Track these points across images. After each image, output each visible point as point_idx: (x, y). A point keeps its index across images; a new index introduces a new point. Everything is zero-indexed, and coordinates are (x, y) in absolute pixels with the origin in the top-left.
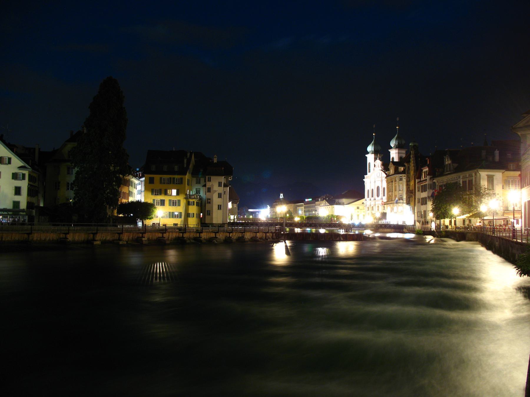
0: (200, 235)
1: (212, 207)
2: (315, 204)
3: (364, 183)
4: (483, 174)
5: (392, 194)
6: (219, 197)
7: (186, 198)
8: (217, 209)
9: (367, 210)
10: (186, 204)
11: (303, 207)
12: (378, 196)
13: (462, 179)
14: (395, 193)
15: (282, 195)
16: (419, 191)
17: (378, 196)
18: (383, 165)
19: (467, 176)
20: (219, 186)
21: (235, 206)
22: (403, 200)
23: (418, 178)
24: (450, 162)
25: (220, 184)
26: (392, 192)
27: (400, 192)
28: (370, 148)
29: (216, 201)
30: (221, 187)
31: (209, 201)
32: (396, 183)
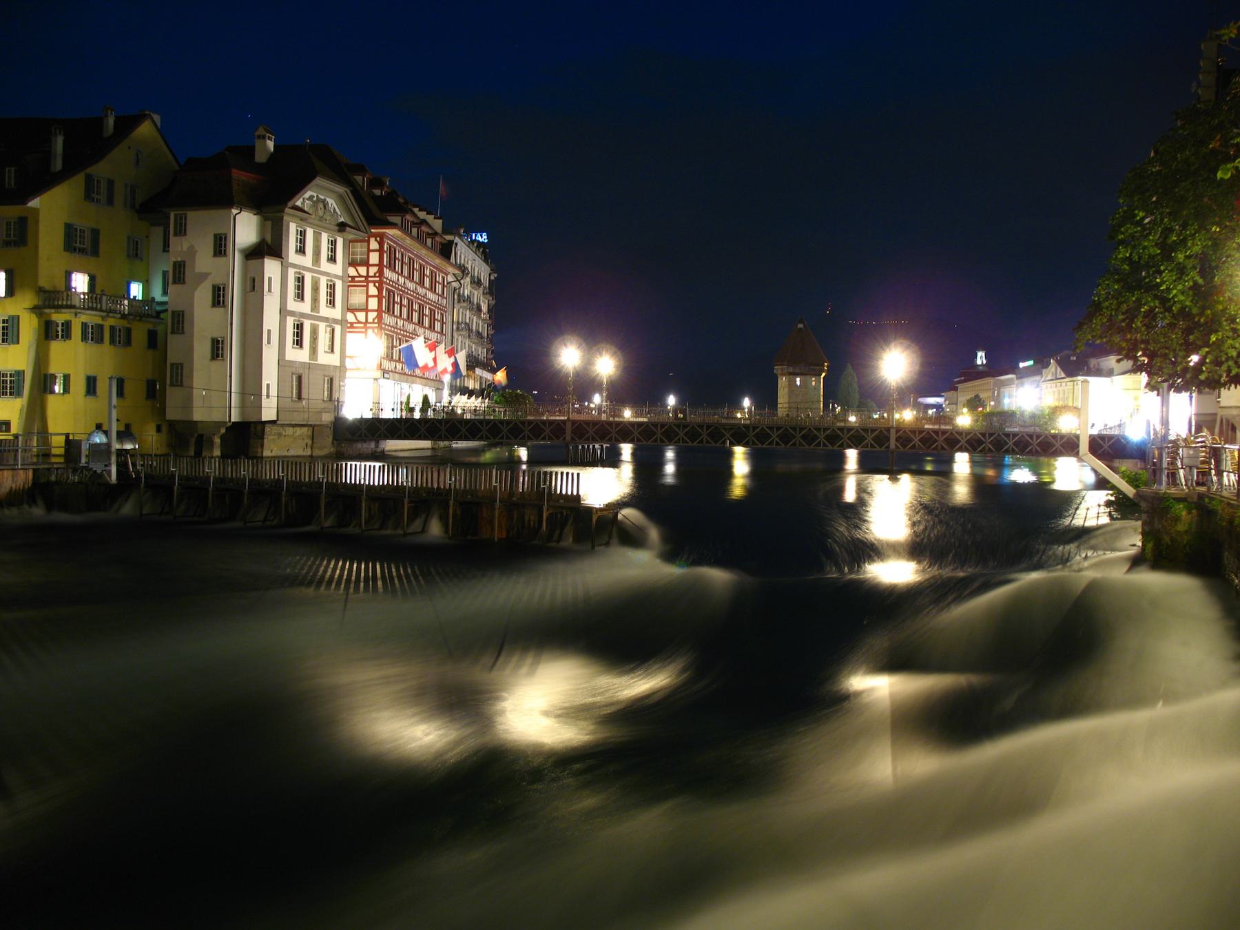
1: (190, 350)
7: (35, 309)
8: (209, 356)
9: (248, 290)
10: (39, 335)
15: (984, 354)
21: (814, 383)
31: (180, 321)
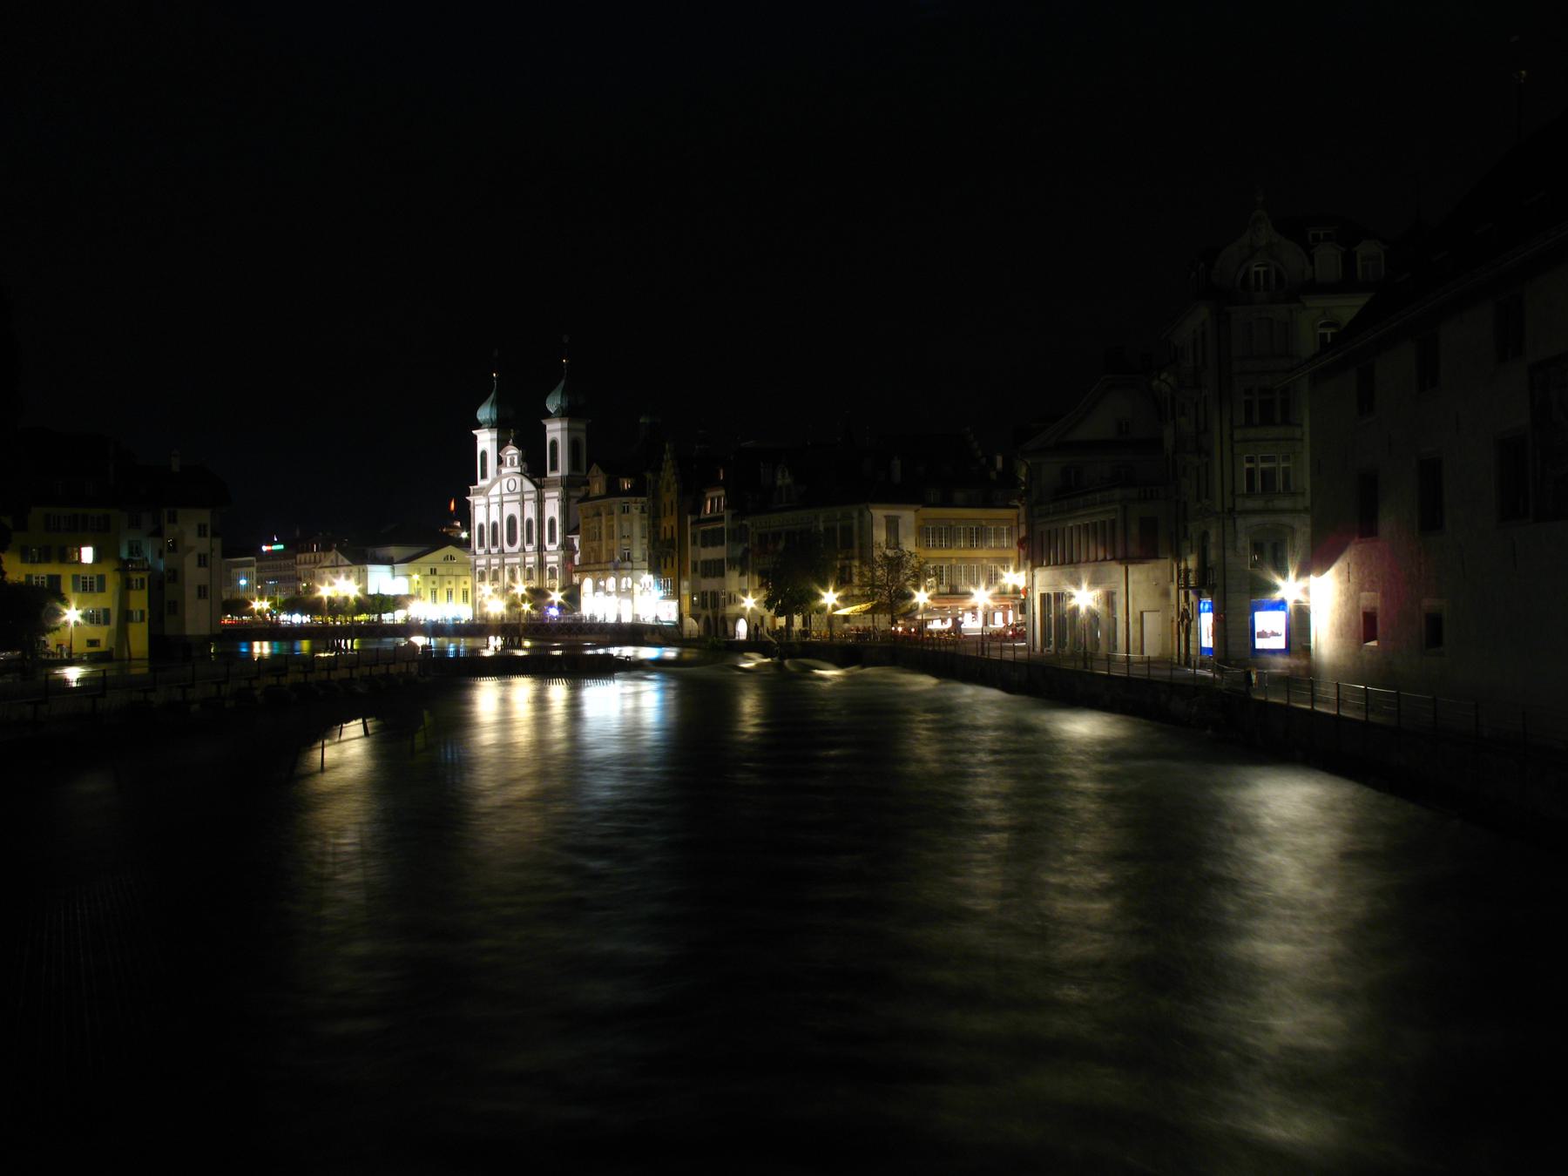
0: (351, 674)
2: (294, 561)
3: (469, 506)
4: (879, 514)
5: (600, 547)
6: (200, 565)
11: (254, 570)
12: (512, 541)
13: (823, 522)
14: (607, 545)
16: (694, 543)
17: (512, 541)
18: (525, 459)
19: (838, 517)
20: (200, 535)
22: (632, 562)
23: (692, 513)
24: (788, 481)
25: (202, 531)
26: (600, 539)
27: (625, 541)
28: (485, 413)
29: (193, 573)
30: (203, 539)
31: (174, 575)
32: (612, 519)
